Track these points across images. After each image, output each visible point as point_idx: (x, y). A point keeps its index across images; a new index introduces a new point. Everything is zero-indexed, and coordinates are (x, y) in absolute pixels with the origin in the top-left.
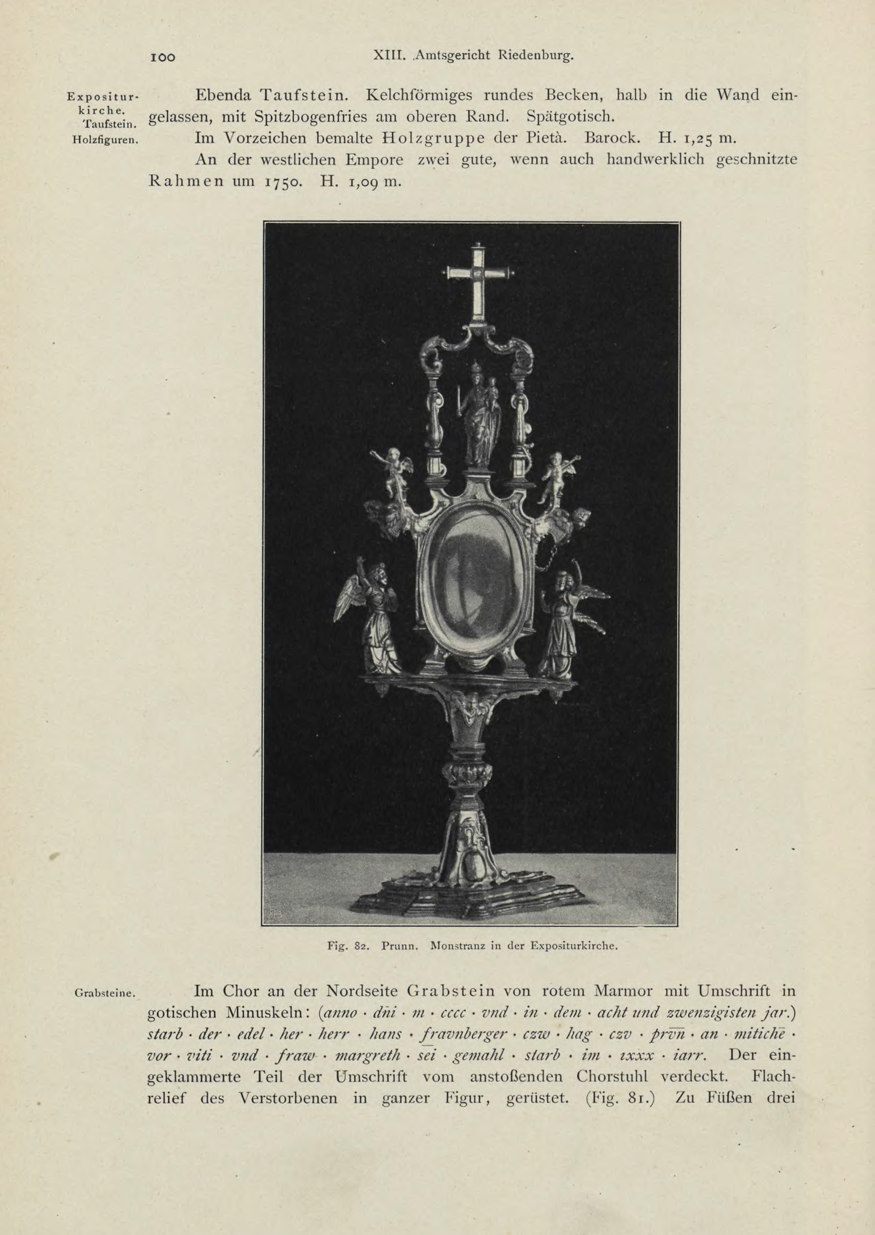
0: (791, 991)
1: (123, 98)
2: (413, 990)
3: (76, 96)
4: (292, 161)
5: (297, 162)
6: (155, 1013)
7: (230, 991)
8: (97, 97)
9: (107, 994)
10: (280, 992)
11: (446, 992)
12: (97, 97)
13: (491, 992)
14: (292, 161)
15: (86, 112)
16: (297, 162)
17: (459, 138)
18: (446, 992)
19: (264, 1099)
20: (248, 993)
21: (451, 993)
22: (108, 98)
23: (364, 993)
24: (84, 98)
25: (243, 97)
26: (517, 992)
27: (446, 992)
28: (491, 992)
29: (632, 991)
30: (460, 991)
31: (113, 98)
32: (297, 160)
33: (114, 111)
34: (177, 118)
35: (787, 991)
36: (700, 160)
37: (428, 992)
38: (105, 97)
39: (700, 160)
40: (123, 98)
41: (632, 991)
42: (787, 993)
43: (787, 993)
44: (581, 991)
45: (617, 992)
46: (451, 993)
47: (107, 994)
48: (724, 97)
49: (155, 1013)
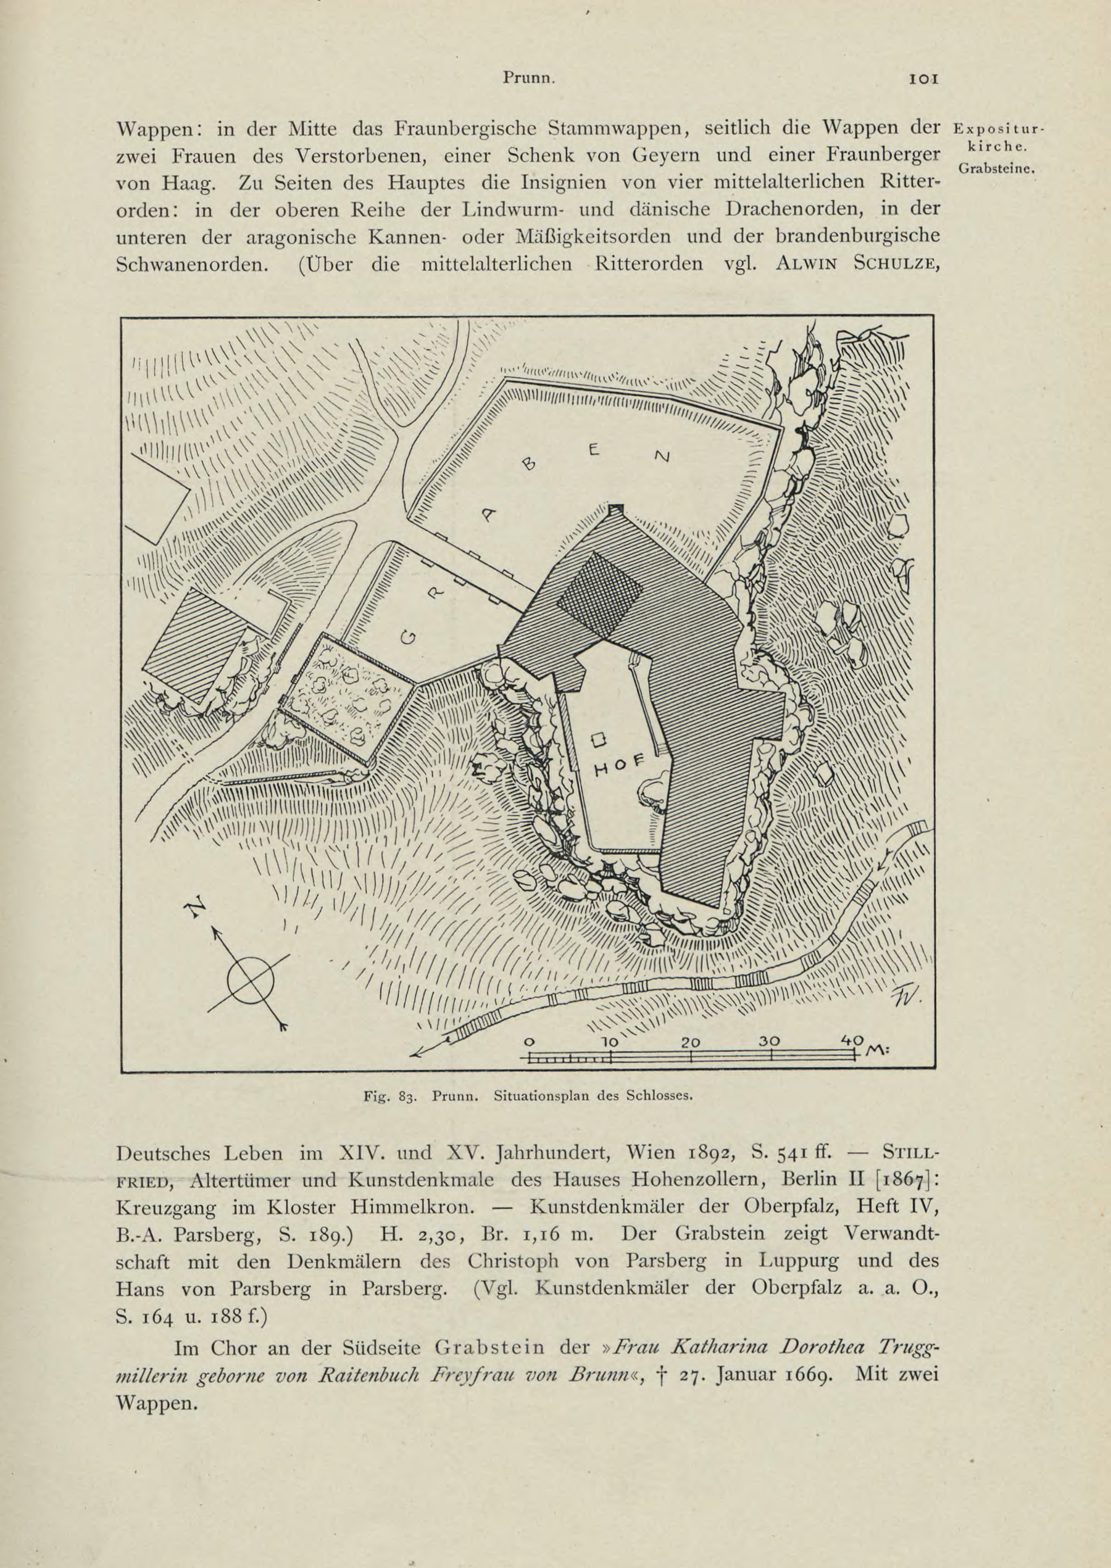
0: (737, 1261)
1: (1025, 130)
2: (442, 1346)
3: (964, 129)
4: (736, 129)
5: (743, 131)
6: (285, 238)
7: (220, 1348)
8: (991, 130)
9: (667, 1097)
10: (284, 1349)
11: (483, 1349)
12: (991, 130)
13: (539, 1349)
14: (736, 129)
15: (977, 148)
16: (743, 131)
17: (154, 130)
18: (483, 1349)
19: (328, 158)
20: (243, 1350)
21: (490, 1349)
22: (1005, 130)
23: (378, 1350)
24: (975, 130)
25: (364, 131)
26: (198, 1291)
27: (482, 1348)
28: (539, 1349)
29: (404, 1208)
30: (501, 1348)
31: (1012, 129)
32: (743, 128)
33: (1014, 148)
34: (374, 131)
35: (731, 1261)
36: (765, 128)
37: (461, 1350)
38: (1001, 129)
39: (765, 128)
40: (1025, 130)
41: (404, 1208)
42: (731, 1263)
43: (731, 1263)
44: (318, 1154)
45: (385, 1290)
46: (490, 1349)
47: (667, 1097)
48: (832, 130)
49: (285, 238)
